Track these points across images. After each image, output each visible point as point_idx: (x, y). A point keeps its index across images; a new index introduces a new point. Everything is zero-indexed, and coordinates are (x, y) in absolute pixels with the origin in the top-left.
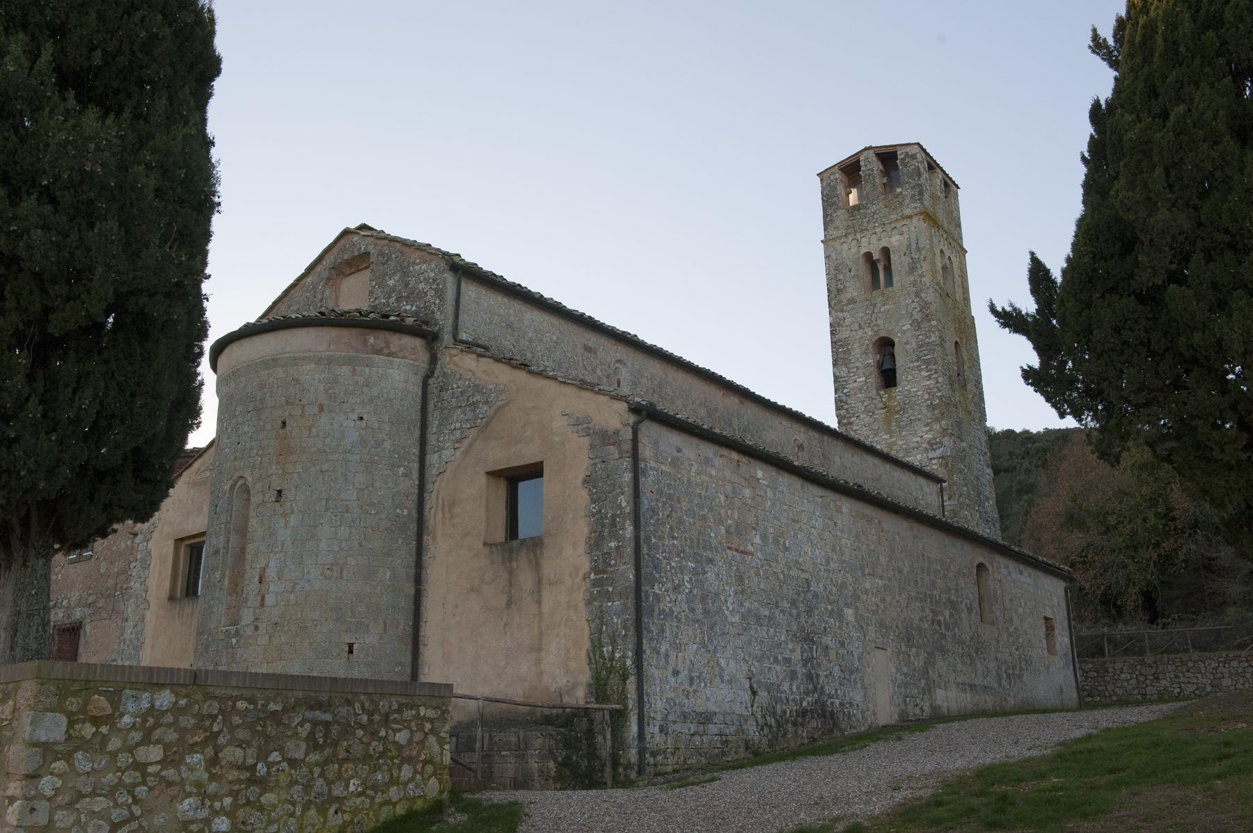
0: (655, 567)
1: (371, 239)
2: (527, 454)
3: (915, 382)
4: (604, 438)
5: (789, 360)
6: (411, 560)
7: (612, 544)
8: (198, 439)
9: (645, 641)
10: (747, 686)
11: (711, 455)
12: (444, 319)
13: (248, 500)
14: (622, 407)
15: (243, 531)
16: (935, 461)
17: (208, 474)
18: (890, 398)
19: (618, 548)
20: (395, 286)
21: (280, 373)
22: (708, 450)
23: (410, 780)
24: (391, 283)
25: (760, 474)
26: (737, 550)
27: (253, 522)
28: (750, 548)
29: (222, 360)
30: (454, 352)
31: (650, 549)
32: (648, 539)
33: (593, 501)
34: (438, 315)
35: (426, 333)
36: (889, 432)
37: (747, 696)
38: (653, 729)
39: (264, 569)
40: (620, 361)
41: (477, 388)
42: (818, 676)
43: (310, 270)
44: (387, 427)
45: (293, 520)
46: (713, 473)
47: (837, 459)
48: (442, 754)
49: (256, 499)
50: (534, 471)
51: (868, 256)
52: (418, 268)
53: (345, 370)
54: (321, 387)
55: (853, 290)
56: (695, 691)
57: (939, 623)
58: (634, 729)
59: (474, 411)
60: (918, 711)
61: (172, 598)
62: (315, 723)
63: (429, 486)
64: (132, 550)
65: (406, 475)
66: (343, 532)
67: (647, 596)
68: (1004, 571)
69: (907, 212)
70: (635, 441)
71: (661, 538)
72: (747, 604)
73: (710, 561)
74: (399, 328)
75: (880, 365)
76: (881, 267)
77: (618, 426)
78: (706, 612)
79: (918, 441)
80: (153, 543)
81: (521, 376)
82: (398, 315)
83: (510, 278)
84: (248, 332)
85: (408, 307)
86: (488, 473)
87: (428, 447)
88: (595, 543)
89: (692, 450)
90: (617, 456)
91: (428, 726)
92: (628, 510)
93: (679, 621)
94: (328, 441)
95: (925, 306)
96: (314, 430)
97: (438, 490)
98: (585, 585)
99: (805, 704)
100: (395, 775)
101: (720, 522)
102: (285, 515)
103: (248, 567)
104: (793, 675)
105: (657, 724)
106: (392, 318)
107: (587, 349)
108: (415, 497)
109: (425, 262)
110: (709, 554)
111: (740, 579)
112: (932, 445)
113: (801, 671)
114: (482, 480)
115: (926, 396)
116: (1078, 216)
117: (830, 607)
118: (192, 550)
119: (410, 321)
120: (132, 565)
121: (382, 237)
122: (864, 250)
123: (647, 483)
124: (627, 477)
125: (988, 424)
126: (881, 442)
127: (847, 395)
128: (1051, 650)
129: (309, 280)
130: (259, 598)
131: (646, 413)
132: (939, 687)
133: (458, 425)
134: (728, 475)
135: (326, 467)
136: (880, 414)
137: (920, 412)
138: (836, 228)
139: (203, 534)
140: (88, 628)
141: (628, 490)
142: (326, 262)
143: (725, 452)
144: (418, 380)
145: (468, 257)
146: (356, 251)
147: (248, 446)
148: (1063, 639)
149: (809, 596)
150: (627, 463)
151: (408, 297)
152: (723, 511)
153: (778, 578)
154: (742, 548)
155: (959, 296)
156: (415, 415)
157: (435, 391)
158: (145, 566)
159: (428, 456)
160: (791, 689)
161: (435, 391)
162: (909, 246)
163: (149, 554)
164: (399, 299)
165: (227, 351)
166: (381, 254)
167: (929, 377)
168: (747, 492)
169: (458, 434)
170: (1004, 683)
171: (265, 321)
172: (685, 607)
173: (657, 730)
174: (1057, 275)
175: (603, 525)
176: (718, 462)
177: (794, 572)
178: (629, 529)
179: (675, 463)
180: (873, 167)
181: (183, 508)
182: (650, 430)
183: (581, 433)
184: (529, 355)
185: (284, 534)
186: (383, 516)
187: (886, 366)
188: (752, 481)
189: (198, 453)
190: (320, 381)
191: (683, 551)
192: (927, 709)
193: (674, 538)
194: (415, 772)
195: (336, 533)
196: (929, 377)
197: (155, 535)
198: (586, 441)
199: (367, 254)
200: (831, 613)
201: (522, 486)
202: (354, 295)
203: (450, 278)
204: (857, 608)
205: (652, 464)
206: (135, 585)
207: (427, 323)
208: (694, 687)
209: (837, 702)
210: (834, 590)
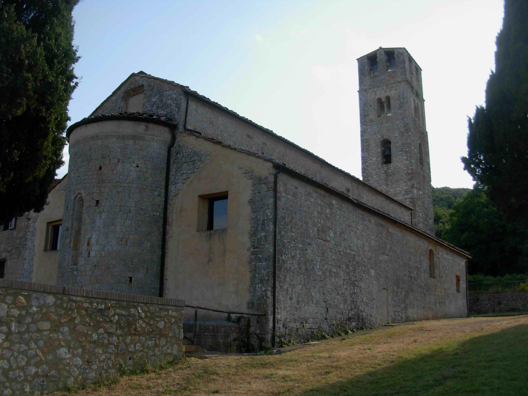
0: (283, 246)
1: (146, 78)
2: (220, 188)
3: (399, 161)
4: (259, 181)
5: (342, 147)
6: (160, 238)
7: (263, 234)
8: (61, 172)
9: (277, 283)
10: (324, 306)
11: (311, 191)
12: (179, 118)
13: (83, 205)
14: (270, 165)
15: (80, 220)
16: (408, 200)
17: (63, 191)
18: (388, 169)
19: (265, 236)
20: (156, 101)
21: (99, 142)
22: (310, 189)
23: (164, 345)
24: (154, 100)
25: (334, 202)
26: (322, 240)
27: (85, 216)
28: (328, 238)
29: (72, 135)
30: (185, 135)
31: (281, 237)
32: (280, 233)
33: (253, 212)
34: (177, 116)
35: (171, 125)
36: (387, 185)
37: (323, 311)
38: (279, 325)
39: (90, 239)
40: (264, 144)
41: (195, 153)
42: (356, 301)
43: (114, 93)
44: (150, 171)
45: (104, 216)
46: (312, 200)
47: (365, 197)
48: (179, 334)
49: (86, 204)
50: (224, 196)
51: (379, 100)
52: (167, 93)
53: (130, 142)
54: (119, 150)
55: (373, 115)
56: (300, 308)
57: (411, 277)
58: (271, 325)
59: (193, 164)
61: (45, 250)
62: (120, 315)
63: (170, 202)
64: (28, 227)
65: (159, 196)
66: (128, 222)
67: (279, 261)
68: (441, 253)
69: (399, 79)
70: (275, 183)
71: (286, 232)
72: (326, 266)
73: (309, 244)
74: (158, 122)
75: (383, 153)
76: (385, 105)
77: (267, 174)
78: (307, 269)
79: (398, 190)
80: (36, 223)
81: (218, 147)
82: (157, 116)
83: (213, 99)
84: (85, 122)
85: (162, 112)
86: (199, 196)
87: (170, 182)
88: (253, 233)
89: (302, 189)
90: (266, 190)
91: (173, 320)
92: (271, 217)
93: (294, 273)
94: (121, 177)
95: (406, 125)
96: (115, 171)
97: (175, 205)
98: (249, 253)
99: (350, 315)
100: (158, 343)
101: (314, 225)
102: (100, 213)
103: (82, 238)
105: (282, 323)
106: (155, 117)
107: (249, 136)
108: (162, 207)
109: (171, 90)
110: (309, 241)
111: (323, 254)
112: (407, 192)
113: (349, 299)
114: (196, 199)
115: (405, 169)
117: (364, 269)
118: (54, 228)
119: (163, 119)
120: (28, 233)
121: (150, 77)
122: (378, 97)
123: (280, 204)
124: (271, 200)
125: (215, 202)
126: (383, 188)
127: (367, 166)
128: (458, 291)
129: (114, 98)
130: (87, 253)
131: (280, 169)
133: (185, 172)
134: (319, 202)
135: (120, 190)
136: (383, 176)
137: (402, 176)
138: (365, 85)
139: (61, 220)
141: (272, 206)
142: (123, 90)
143: (318, 190)
144: (165, 148)
145: (192, 89)
146: (138, 85)
147: (83, 178)
148: (463, 285)
149: (355, 263)
150: (271, 193)
151: (162, 107)
152: (316, 220)
153: (341, 255)
154: (324, 239)
156: (164, 165)
157: (174, 154)
158: (34, 235)
159: (170, 186)
160: (344, 308)
161: (174, 154)
162: (399, 96)
163: (35, 229)
164: (158, 108)
165: (74, 131)
166: (150, 86)
167: (407, 159)
168: (328, 211)
169: (185, 176)
170: (438, 305)
171: (93, 117)
172: (296, 266)
173: (281, 326)
175: (258, 224)
176: (314, 195)
177: (348, 251)
178: (272, 227)
179: (295, 195)
180: (382, 58)
181: (55, 206)
182: (283, 177)
183: (248, 178)
184: (220, 138)
185: (99, 222)
186: (147, 216)
187: (387, 153)
188: (331, 206)
189: (60, 181)
190: (118, 148)
191: (297, 239)
192: (404, 318)
193: (292, 232)
194: (167, 342)
195: (124, 223)
196: (407, 159)
197: (38, 220)
198: (250, 182)
199: (143, 86)
201: (216, 203)
202: (136, 105)
203: (183, 97)
204: (376, 270)
205: (283, 194)
206: (29, 243)
207: (171, 120)
208: (299, 306)
209: (365, 314)
210: (366, 260)
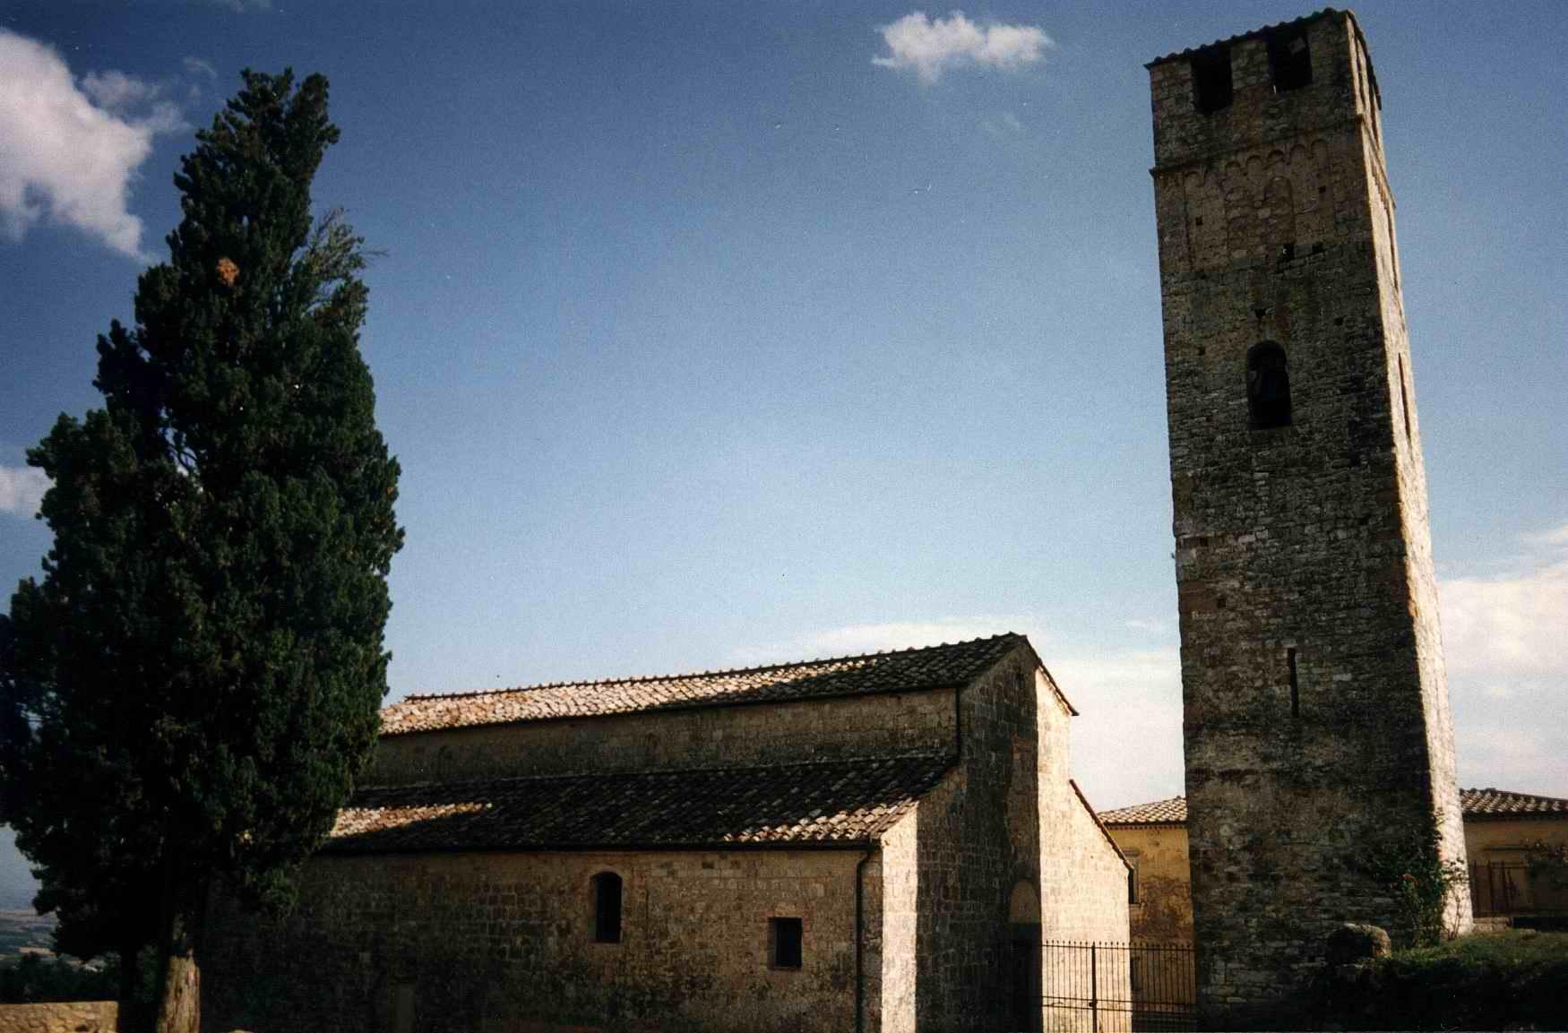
140: (763, 956)
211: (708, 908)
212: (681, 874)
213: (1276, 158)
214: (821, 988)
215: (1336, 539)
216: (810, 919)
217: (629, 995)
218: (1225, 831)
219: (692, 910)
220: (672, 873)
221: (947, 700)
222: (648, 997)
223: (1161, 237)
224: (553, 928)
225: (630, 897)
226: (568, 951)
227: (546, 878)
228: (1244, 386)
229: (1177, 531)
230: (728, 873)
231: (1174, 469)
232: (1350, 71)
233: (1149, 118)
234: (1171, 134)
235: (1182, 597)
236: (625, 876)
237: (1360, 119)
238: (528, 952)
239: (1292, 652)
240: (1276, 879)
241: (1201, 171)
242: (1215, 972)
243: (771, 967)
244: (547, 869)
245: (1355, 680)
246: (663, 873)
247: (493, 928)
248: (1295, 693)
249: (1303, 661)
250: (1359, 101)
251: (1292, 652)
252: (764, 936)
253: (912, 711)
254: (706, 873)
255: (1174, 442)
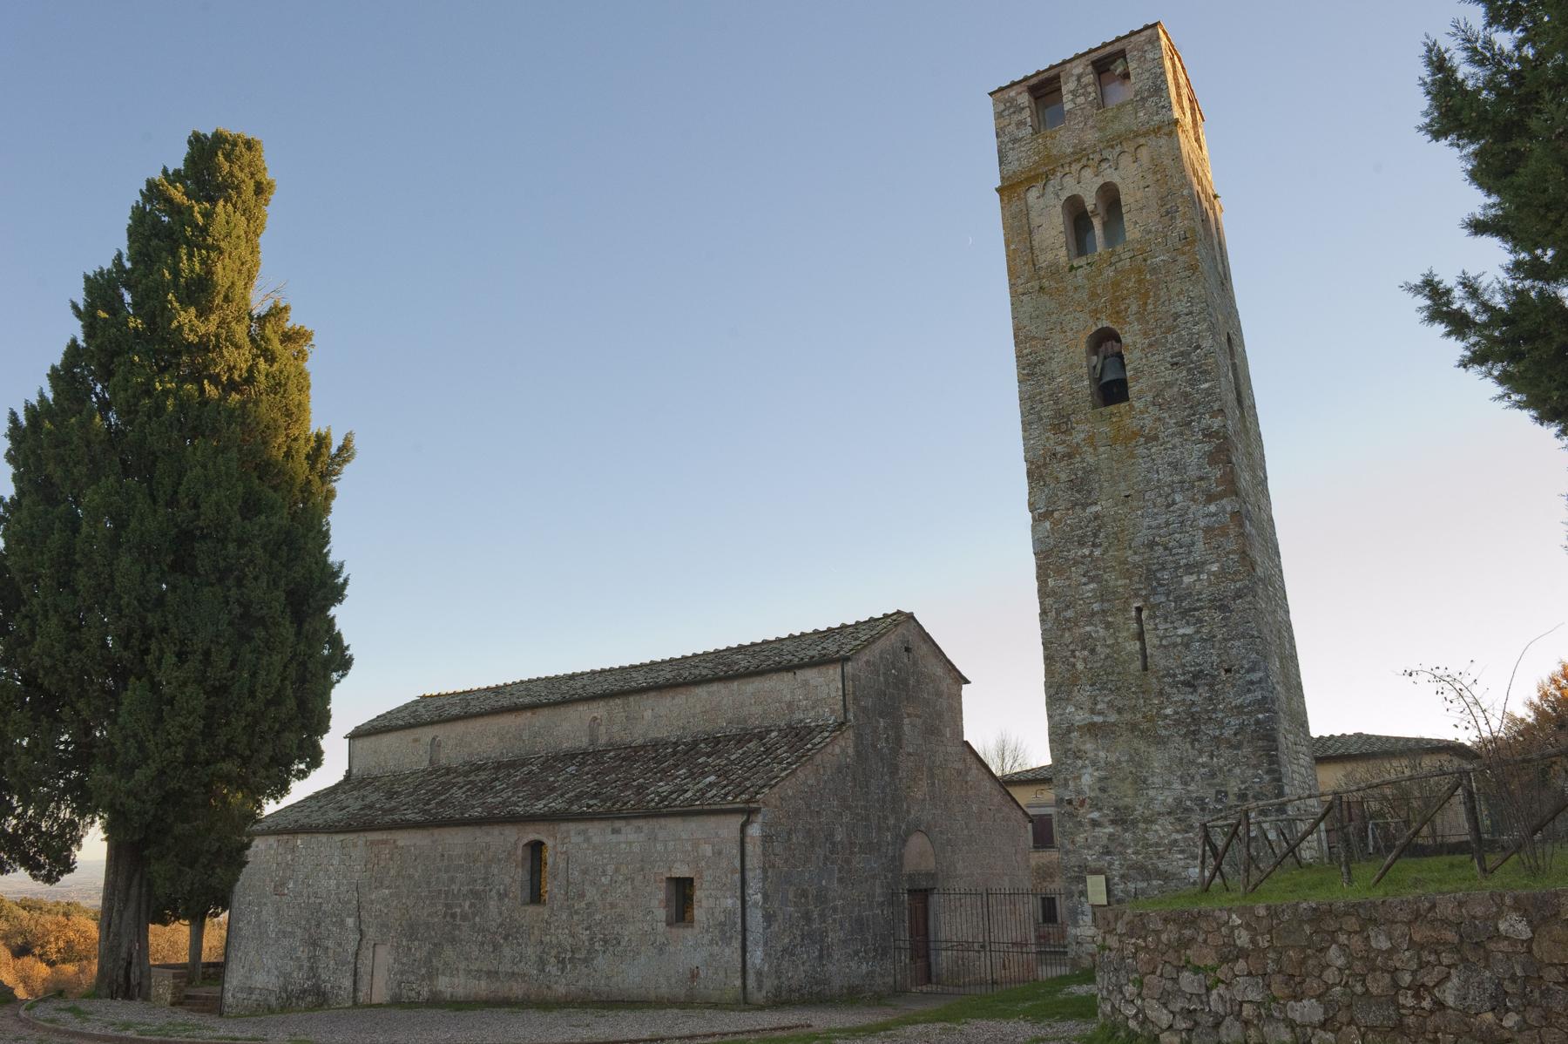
60: (413, 994)
104: (300, 968)
113: (306, 964)
116: (184, 155)
132: (443, 974)
140: (661, 914)
155: (1395, 769)
174: (82, 307)
200: (334, 924)
211: (617, 870)
212: (596, 840)
213: (1105, 165)
214: (711, 942)
215: (1174, 503)
216: (701, 877)
217: (554, 952)
218: (1086, 780)
219: (604, 873)
220: (588, 840)
221: (834, 672)
222: (569, 955)
223: (1007, 246)
224: (493, 893)
225: (555, 863)
226: (506, 914)
227: (488, 847)
228: (1085, 370)
229: (1032, 507)
230: (632, 837)
231: (1026, 451)
232: (1165, 81)
233: (993, 143)
234: (1011, 156)
235: (1039, 567)
236: (549, 843)
237: (1176, 122)
238: (475, 915)
239: (1139, 610)
240: (1134, 823)
241: (1040, 184)
242: (1083, 913)
243: (669, 924)
244: (488, 839)
245: (1197, 632)
246: (580, 839)
247: (447, 893)
248: (1143, 649)
249: (1150, 617)
250: (1176, 108)
251: (1139, 610)
252: (662, 895)
253: (806, 683)
254: (614, 838)
255: (1026, 425)
